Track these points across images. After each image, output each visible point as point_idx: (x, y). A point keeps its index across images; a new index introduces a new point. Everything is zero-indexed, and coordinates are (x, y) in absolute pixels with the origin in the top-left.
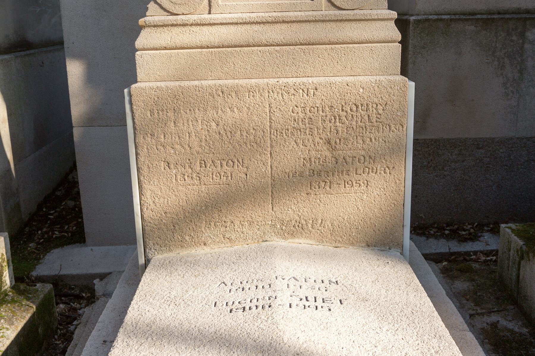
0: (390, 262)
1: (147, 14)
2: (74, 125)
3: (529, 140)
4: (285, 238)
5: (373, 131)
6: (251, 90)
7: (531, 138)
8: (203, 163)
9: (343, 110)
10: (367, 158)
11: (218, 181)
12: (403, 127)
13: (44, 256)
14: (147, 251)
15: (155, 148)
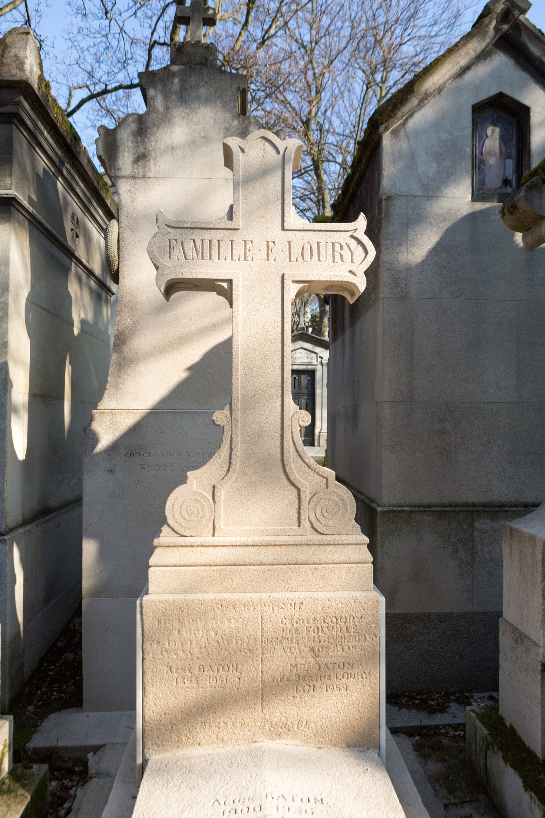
0: (369, 769)
1: (161, 535)
2: (83, 596)
3: (484, 615)
4: (273, 739)
5: (351, 641)
6: (246, 604)
7: (486, 613)
8: (202, 668)
9: (324, 622)
10: (346, 665)
11: (214, 684)
12: (376, 637)
13: (41, 723)
14: (146, 750)
15: (160, 654)
